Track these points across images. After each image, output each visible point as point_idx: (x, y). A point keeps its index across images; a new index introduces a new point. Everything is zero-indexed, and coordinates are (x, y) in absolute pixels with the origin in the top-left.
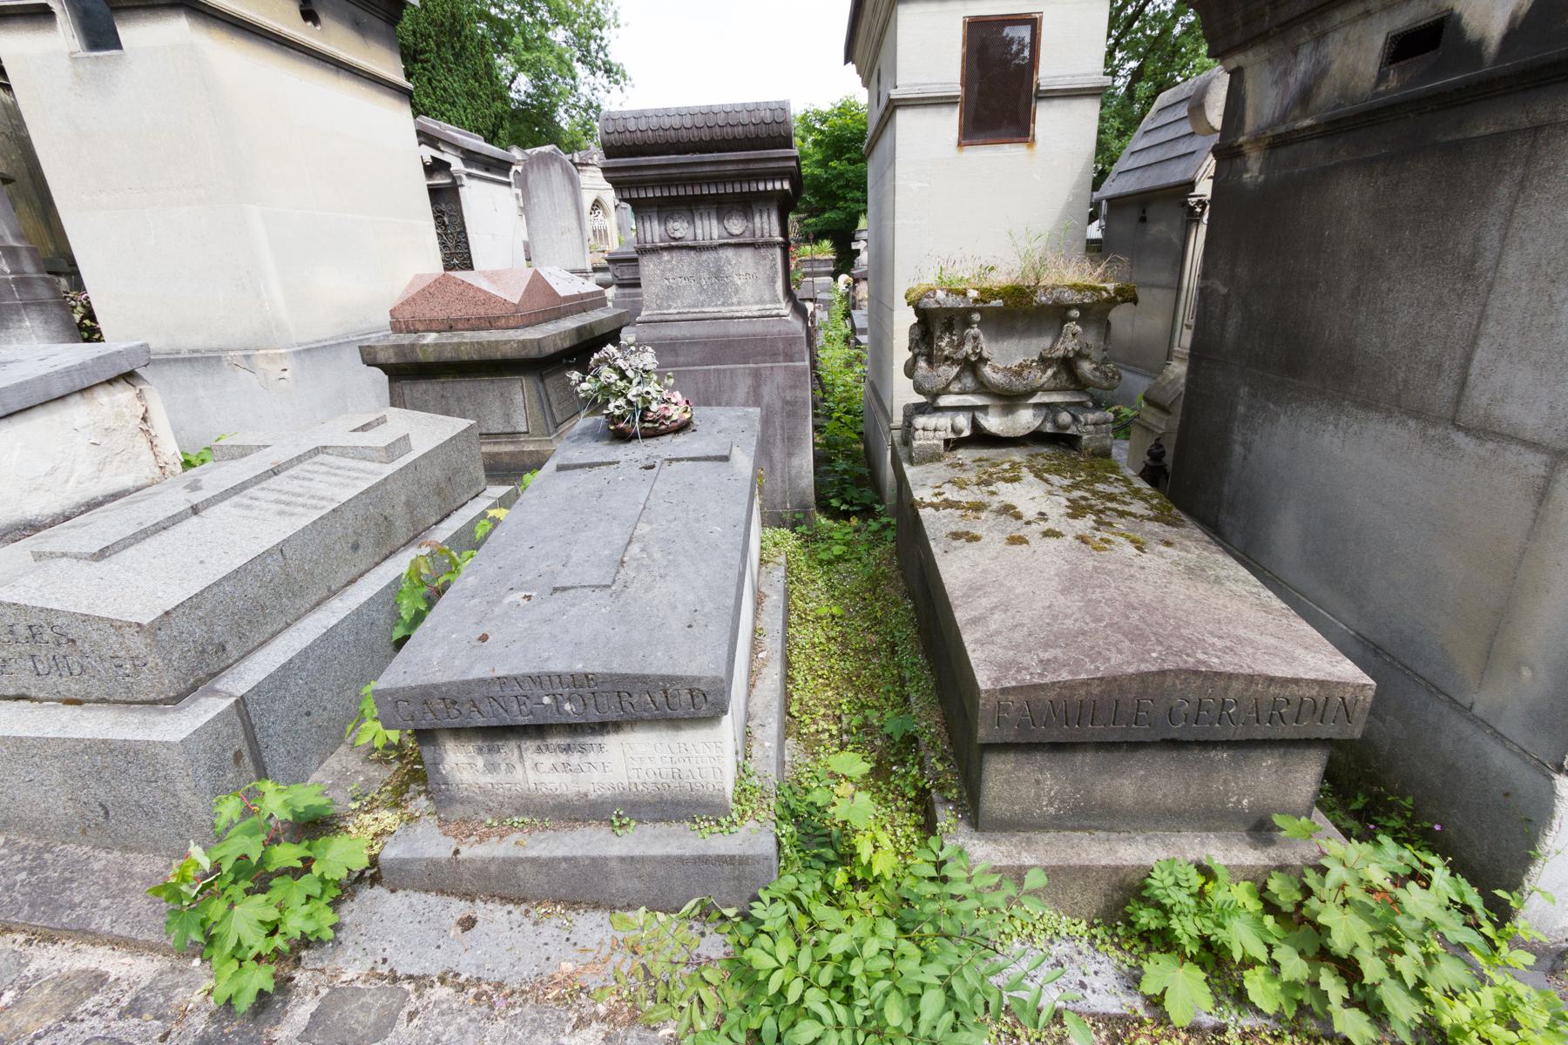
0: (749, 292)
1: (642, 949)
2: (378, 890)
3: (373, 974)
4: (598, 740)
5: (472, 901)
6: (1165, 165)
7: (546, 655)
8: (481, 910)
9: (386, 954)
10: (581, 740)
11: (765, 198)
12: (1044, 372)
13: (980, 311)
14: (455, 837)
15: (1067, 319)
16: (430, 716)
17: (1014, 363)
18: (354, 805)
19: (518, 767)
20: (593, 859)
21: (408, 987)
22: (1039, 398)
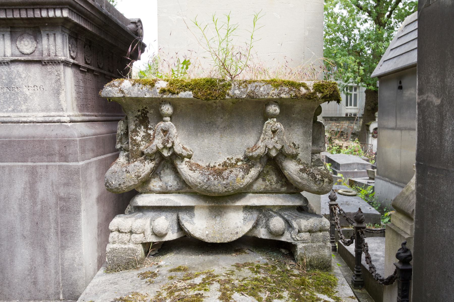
0: (36, 101)
6: (410, 53)
11: (52, 25)
12: (247, 171)
13: (170, 102)
15: (266, 117)
17: (218, 161)
22: (253, 200)
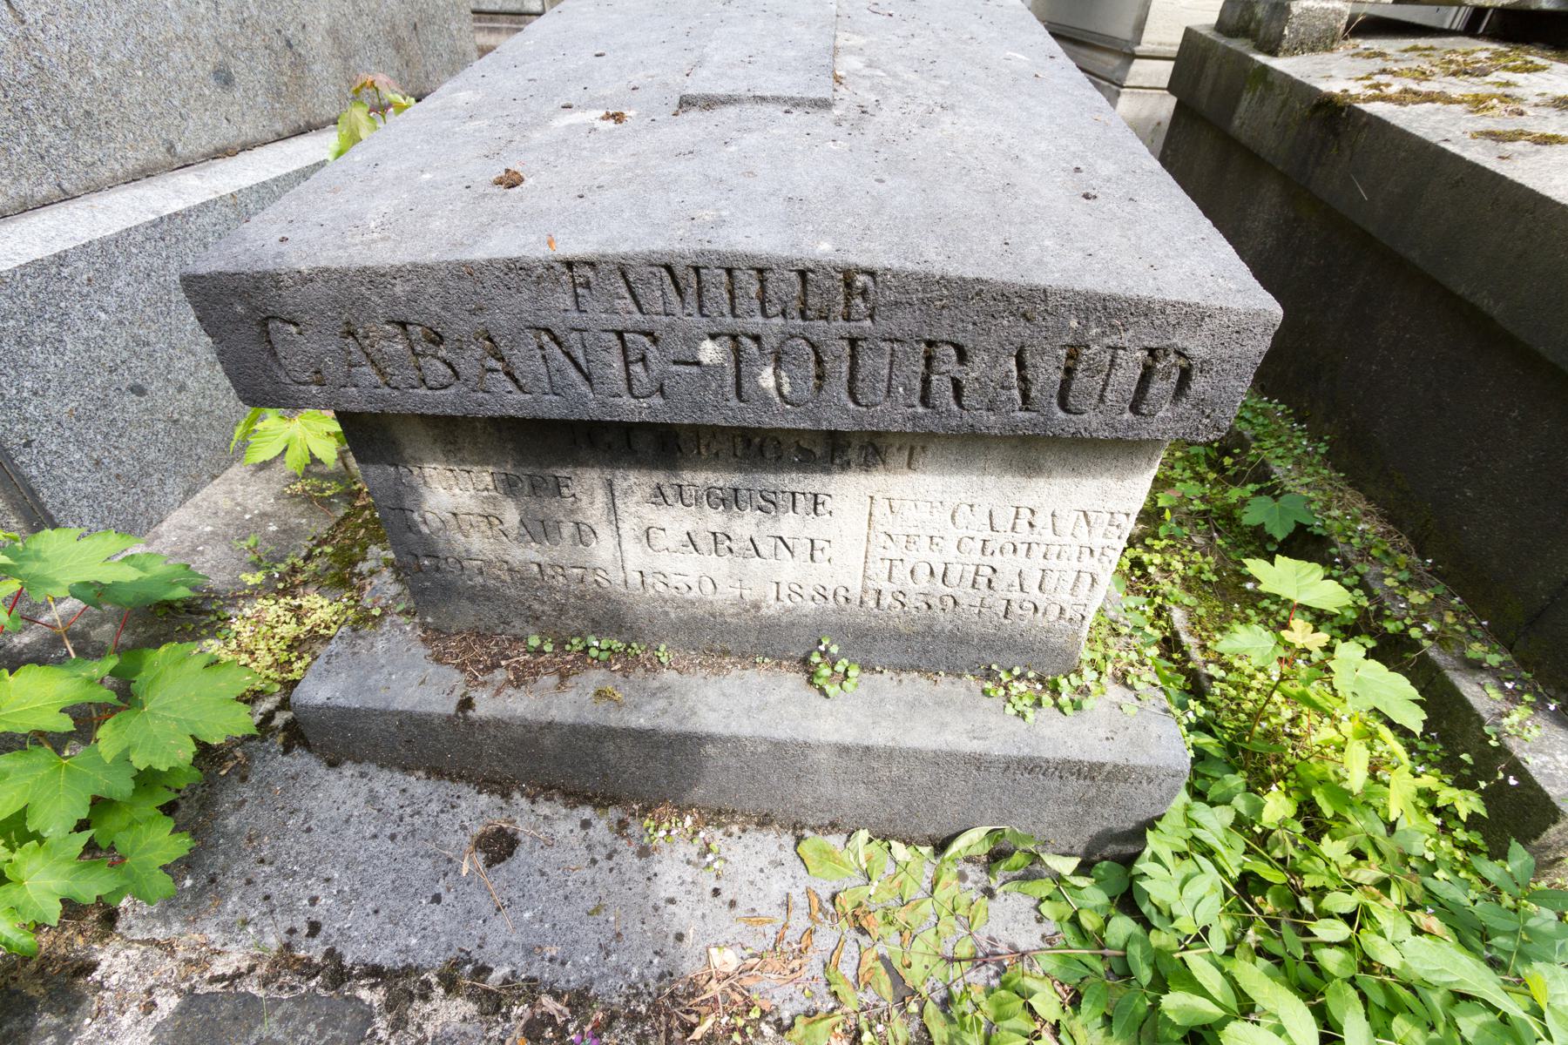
1: (875, 924)
2: (300, 760)
3: (286, 959)
4: (815, 482)
5: (506, 796)
7: (708, 215)
8: (528, 816)
9: (318, 913)
10: (770, 480)
14: (462, 668)
16: (368, 374)
18: (254, 579)
19: (605, 533)
20: (778, 746)
21: (371, 996)
